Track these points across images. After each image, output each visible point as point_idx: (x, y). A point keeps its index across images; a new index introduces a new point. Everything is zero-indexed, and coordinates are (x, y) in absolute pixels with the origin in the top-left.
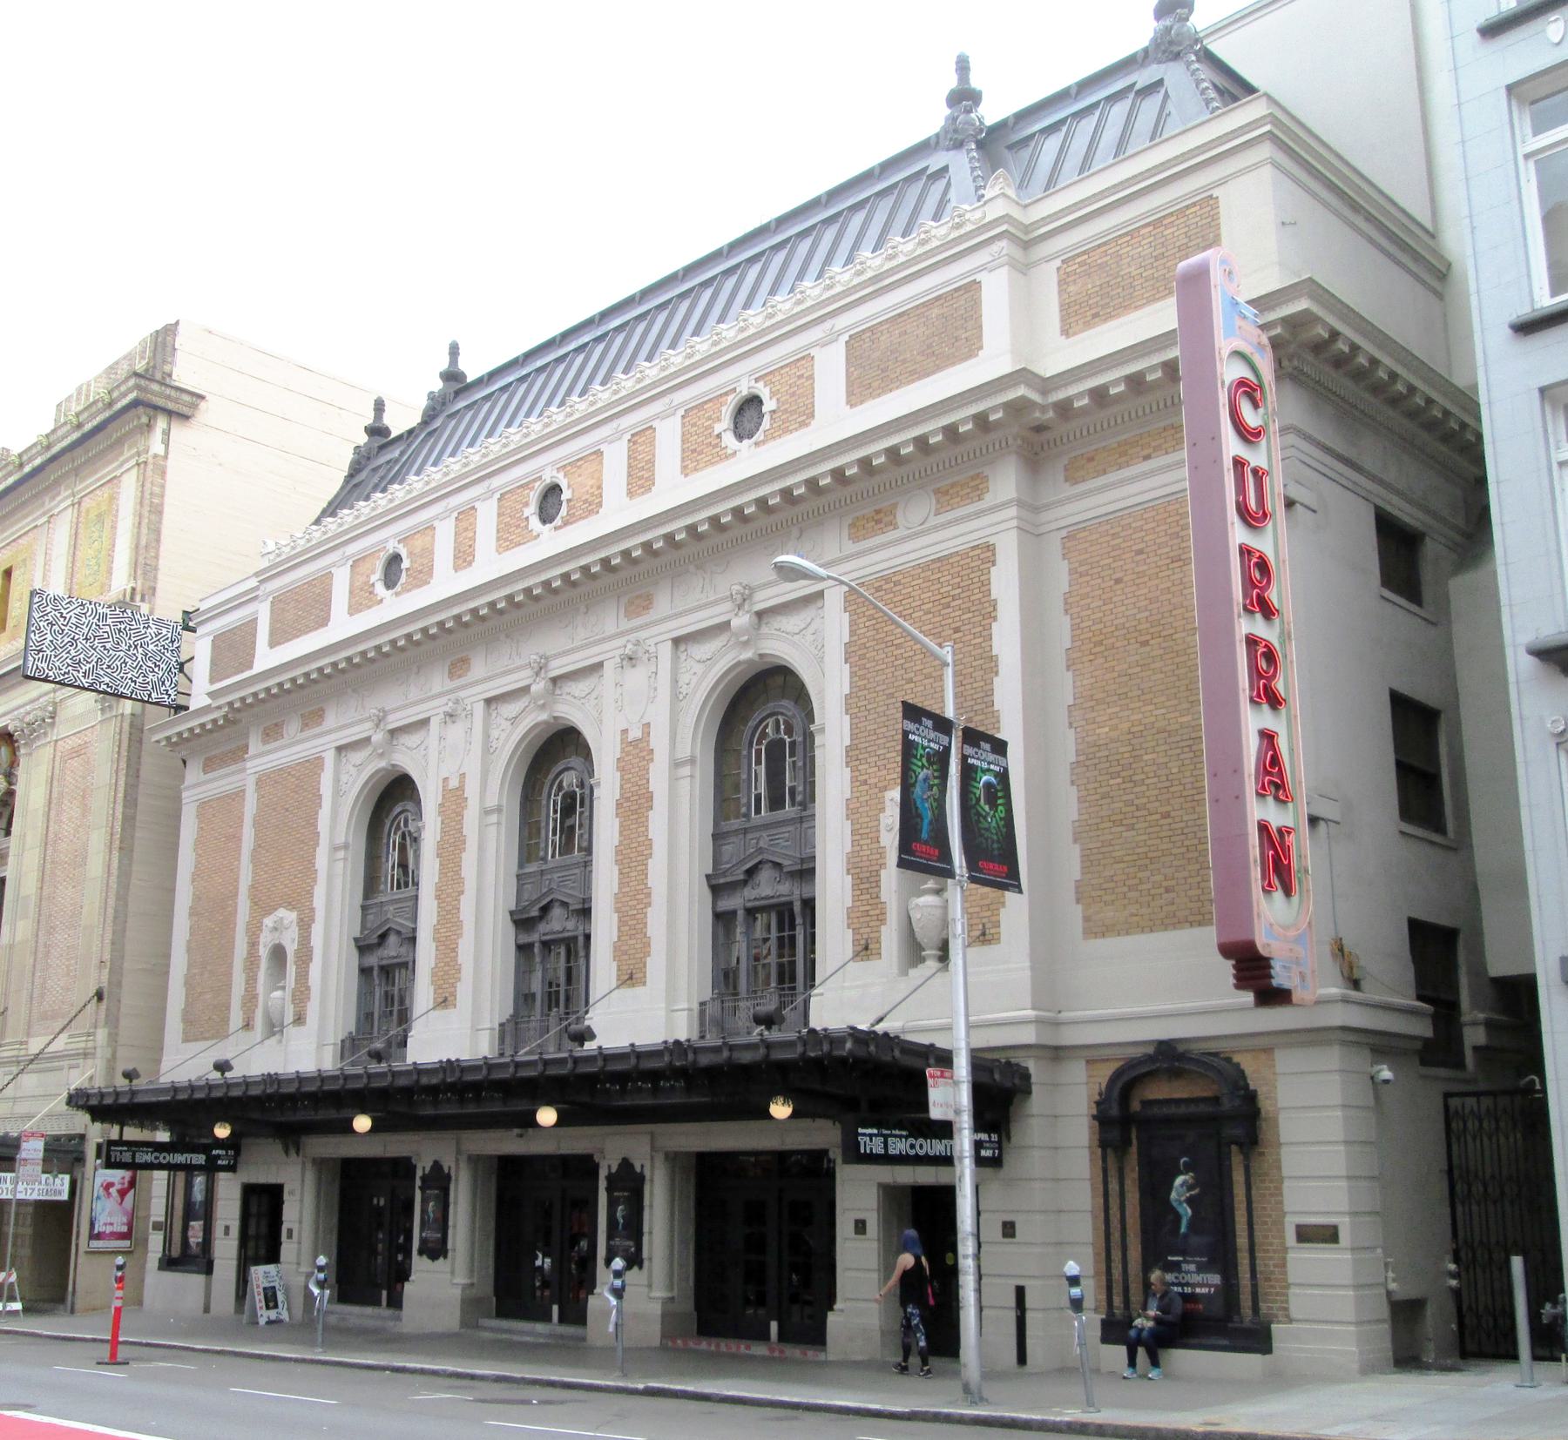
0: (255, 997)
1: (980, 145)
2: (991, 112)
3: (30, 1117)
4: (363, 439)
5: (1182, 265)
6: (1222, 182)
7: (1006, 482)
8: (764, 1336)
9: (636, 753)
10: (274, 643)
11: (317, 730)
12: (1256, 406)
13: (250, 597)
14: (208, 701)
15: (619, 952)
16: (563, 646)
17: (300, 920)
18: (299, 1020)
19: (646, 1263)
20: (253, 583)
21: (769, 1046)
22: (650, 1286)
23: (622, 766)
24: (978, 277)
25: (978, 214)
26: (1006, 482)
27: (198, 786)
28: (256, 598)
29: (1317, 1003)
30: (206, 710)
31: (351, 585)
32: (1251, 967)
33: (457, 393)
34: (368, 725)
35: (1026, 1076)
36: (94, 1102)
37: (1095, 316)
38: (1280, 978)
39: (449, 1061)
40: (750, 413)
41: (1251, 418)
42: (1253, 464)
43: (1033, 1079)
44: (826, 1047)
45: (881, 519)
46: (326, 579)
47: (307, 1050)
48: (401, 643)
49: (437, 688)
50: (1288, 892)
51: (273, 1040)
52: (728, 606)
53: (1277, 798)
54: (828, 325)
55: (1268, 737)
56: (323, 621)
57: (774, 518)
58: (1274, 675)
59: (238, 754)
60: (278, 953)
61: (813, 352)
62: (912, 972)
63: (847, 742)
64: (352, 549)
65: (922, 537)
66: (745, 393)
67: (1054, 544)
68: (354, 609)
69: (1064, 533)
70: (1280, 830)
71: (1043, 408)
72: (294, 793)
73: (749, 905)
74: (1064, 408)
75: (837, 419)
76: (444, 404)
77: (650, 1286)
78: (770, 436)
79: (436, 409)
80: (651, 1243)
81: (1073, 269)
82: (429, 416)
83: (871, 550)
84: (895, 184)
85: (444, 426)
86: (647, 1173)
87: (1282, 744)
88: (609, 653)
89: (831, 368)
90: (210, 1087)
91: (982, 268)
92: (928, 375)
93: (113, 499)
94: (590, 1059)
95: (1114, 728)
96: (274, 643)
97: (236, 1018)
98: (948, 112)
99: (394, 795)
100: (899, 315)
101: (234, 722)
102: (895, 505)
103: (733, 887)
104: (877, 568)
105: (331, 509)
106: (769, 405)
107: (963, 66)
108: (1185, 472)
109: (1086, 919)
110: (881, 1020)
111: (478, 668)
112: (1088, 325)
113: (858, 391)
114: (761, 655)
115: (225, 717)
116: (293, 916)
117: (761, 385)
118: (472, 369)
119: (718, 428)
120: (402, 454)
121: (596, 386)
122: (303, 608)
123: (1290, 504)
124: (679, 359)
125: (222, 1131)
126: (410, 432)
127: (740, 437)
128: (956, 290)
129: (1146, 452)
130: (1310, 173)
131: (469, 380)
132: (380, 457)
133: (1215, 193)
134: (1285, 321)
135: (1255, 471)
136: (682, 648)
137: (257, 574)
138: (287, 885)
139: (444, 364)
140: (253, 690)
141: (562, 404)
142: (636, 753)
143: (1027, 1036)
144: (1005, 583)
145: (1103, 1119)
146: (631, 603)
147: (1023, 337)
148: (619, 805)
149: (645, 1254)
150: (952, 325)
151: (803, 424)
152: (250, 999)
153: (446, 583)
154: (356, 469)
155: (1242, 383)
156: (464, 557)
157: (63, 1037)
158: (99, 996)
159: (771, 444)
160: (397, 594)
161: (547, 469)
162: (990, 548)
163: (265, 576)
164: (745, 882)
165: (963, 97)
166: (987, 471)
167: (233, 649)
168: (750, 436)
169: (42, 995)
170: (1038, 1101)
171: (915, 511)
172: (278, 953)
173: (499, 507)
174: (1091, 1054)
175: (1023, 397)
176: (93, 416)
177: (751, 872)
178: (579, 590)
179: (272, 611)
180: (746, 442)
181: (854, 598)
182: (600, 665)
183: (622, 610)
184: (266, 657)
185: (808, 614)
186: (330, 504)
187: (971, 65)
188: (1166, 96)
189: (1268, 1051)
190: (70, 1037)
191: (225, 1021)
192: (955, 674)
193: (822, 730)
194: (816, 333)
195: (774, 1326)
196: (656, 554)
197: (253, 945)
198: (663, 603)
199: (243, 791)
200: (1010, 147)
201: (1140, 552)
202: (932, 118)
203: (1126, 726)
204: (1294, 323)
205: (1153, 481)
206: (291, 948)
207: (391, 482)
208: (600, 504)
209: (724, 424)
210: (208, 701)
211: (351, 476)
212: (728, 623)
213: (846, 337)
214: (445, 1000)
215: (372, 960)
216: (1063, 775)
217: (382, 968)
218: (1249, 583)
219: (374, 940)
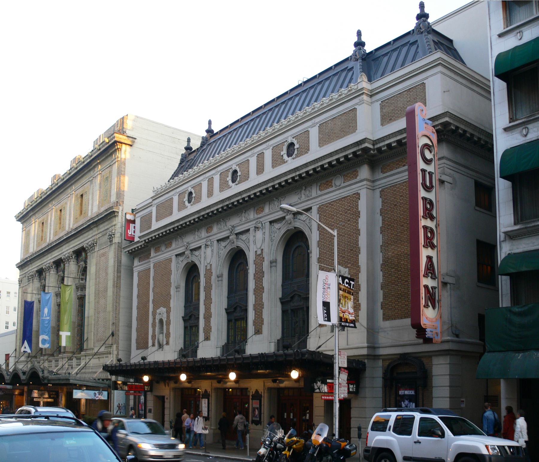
0: (155, 335)
1: (363, 60)
2: (369, 48)
3: (95, 373)
5: (408, 108)
6: (427, 78)
7: (364, 172)
9: (260, 257)
10: (157, 220)
11: (170, 249)
12: (431, 152)
13: (149, 205)
14: (138, 239)
15: (255, 323)
16: (238, 223)
18: (168, 343)
20: (151, 200)
21: (286, 355)
23: (255, 263)
24: (356, 107)
25: (356, 87)
26: (364, 172)
27: (138, 266)
29: (442, 342)
30: (138, 242)
32: (421, 331)
33: (211, 137)
34: (184, 248)
35: (364, 364)
36: (110, 369)
37: (391, 119)
38: (429, 334)
39: (262, 353)
41: (428, 155)
42: (428, 171)
43: (367, 366)
44: (300, 356)
45: (329, 184)
47: (168, 354)
48: (258, 194)
49: (314, 194)
50: (434, 308)
51: (161, 349)
52: (229, 232)
53: (431, 278)
54: (313, 121)
55: (429, 258)
56: (171, 214)
57: (326, 172)
58: (433, 238)
59: (148, 256)
60: (161, 321)
61: (309, 129)
63: (318, 256)
64: (178, 190)
65: (338, 191)
66: (290, 142)
67: (378, 192)
68: (179, 210)
69: (380, 189)
70: (432, 287)
71: (374, 150)
72: (164, 269)
74: (379, 150)
75: (316, 151)
76: (207, 140)
78: (297, 156)
79: (205, 142)
80: (264, 416)
81: (384, 104)
82: (203, 144)
84: (338, 73)
85: (207, 148)
86: (263, 395)
87: (435, 260)
89: (314, 134)
90: (140, 365)
92: (341, 138)
93: (110, 172)
95: (393, 253)
96: (157, 220)
98: (354, 49)
99: (192, 272)
100: (334, 118)
101: (147, 246)
102: (332, 180)
105: (176, 174)
107: (359, 34)
108: (407, 173)
109: (384, 314)
110: (320, 347)
111: (215, 229)
112: (388, 123)
113: (322, 142)
115: (144, 244)
116: (165, 310)
117: (294, 139)
118: (216, 128)
120: (195, 157)
121: (275, 124)
122: (165, 209)
123: (442, 182)
125: (146, 378)
126: (198, 149)
127: (288, 156)
128: (350, 111)
130: (455, 74)
131: (215, 132)
132: (189, 158)
133: (425, 82)
134: (441, 124)
135: (429, 173)
136: (272, 224)
137: (152, 198)
138: (163, 300)
139: (207, 127)
140: (151, 236)
141: (264, 130)
143: (365, 352)
144: (362, 205)
145: (385, 378)
147: (370, 126)
149: (262, 420)
150: (349, 121)
151: (307, 153)
152: (154, 336)
153: (254, 180)
154: (182, 161)
155: (426, 145)
156: (210, 194)
157: (103, 348)
158: (113, 334)
160: (192, 205)
161: (233, 165)
162: (358, 194)
163: (154, 198)
164: (290, 301)
165: (360, 44)
167: (146, 221)
169: (97, 334)
170: (368, 373)
171: (338, 181)
172: (161, 321)
173: (220, 177)
174: (385, 358)
175: (366, 147)
176: (103, 146)
177: (292, 298)
178: (285, 188)
180: (290, 158)
184: (155, 225)
185: (247, 234)
186: (173, 175)
187: (362, 34)
188: (418, 46)
189: (430, 357)
190: (106, 347)
191: (147, 343)
194: (264, 146)
197: (154, 319)
200: (373, 60)
201: (402, 196)
202: (349, 51)
203: (396, 252)
204: (446, 125)
205: (399, 175)
206: (165, 320)
208: (249, 177)
210: (138, 239)
211: (180, 164)
213: (318, 125)
214: (207, 338)
216: (378, 267)
217: (292, 310)
218: (425, 209)
219: (188, 318)
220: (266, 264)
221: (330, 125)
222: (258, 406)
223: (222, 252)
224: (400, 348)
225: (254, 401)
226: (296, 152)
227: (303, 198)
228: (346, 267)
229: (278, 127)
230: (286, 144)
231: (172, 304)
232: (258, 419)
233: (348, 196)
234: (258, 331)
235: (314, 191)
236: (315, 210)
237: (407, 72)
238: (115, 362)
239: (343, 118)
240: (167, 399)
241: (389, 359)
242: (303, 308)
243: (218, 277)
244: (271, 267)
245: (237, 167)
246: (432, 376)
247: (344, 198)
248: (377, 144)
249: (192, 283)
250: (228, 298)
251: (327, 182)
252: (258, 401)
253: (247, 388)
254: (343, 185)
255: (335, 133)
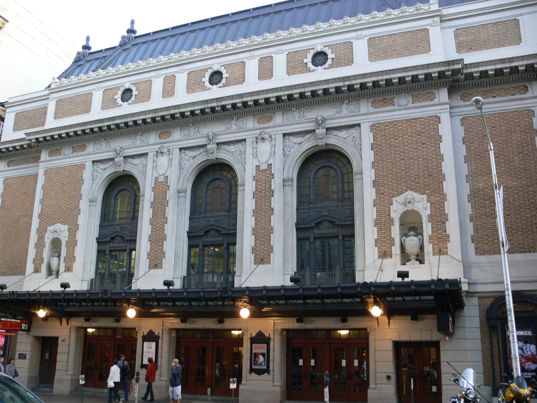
0: (42, 259)
4: (81, 50)
6: (521, 15)
8: (206, 394)
13: (45, 98)
14: (25, 136)
17: (69, 230)
19: (271, 372)
22: (273, 381)
26: (443, 95)
28: (48, 98)
31: (103, 98)
39: (13, 292)
40: (128, 94)
46: (89, 95)
52: (114, 153)
60: (56, 244)
62: (49, 278)
67: (458, 120)
69: (462, 117)
73: (315, 236)
75: (97, 113)
77: (273, 381)
83: (380, 112)
88: (151, 150)
91: (275, 53)
94: (6, 295)
97: (30, 267)
100: (392, 35)
102: (62, 149)
103: (105, 243)
104: (388, 118)
105: (66, 74)
106: (135, 92)
109: (476, 248)
114: (326, 144)
117: (223, 68)
119: (203, 80)
124: (124, 69)
129: (494, 95)
142: (161, 187)
146: (374, 102)
148: (254, 194)
149: (271, 368)
150: (420, 41)
159: (134, 105)
166: (171, 130)
168: (127, 101)
171: (67, 151)
172: (56, 244)
173: (188, 77)
174: (482, 297)
179: (164, 84)
180: (125, 103)
181: (374, 128)
182: (147, 154)
183: (47, 153)
192: (495, 153)
193: (144, 196)
195: (209, 390)
196: (54, 139)
197: (41, 238)
198: (90, 148)
199: (37, 175)
207: (108, 65)
209: (206, 79)
210: (25, 136)
212: (314, 131)
215: (107, 248)
220: (171, 194)
221: (386, 40)
222: (265, 351)
223: (187, 163)
224: (494, 285)
225: (146, 344)
226: (133, 98)
227: (138, 142)
228: (422, 193)
229: (85, 77)
230: (210, 72)
231: (82, 220)
232: (265, 367)
233: (420, 118)
234: (262, 260)
235: (365, 107)
236: (365, 128)
237: (477, 8)
238: (161, 287)
239: (407, 36)
240: (63, 341)
241: (492, 297)
242: (105, 251)
243: (90, 202)
244: (284, 186)
245: (223, 68)
246: (480, 316)
247: (414, 119)
248: (467, 68)
249: (116, 197)
250: (190, 219)
251: (384, 99)
252: (265, 345)
253: (134, 329)
254: (410, 105)
255: (395, 50)
